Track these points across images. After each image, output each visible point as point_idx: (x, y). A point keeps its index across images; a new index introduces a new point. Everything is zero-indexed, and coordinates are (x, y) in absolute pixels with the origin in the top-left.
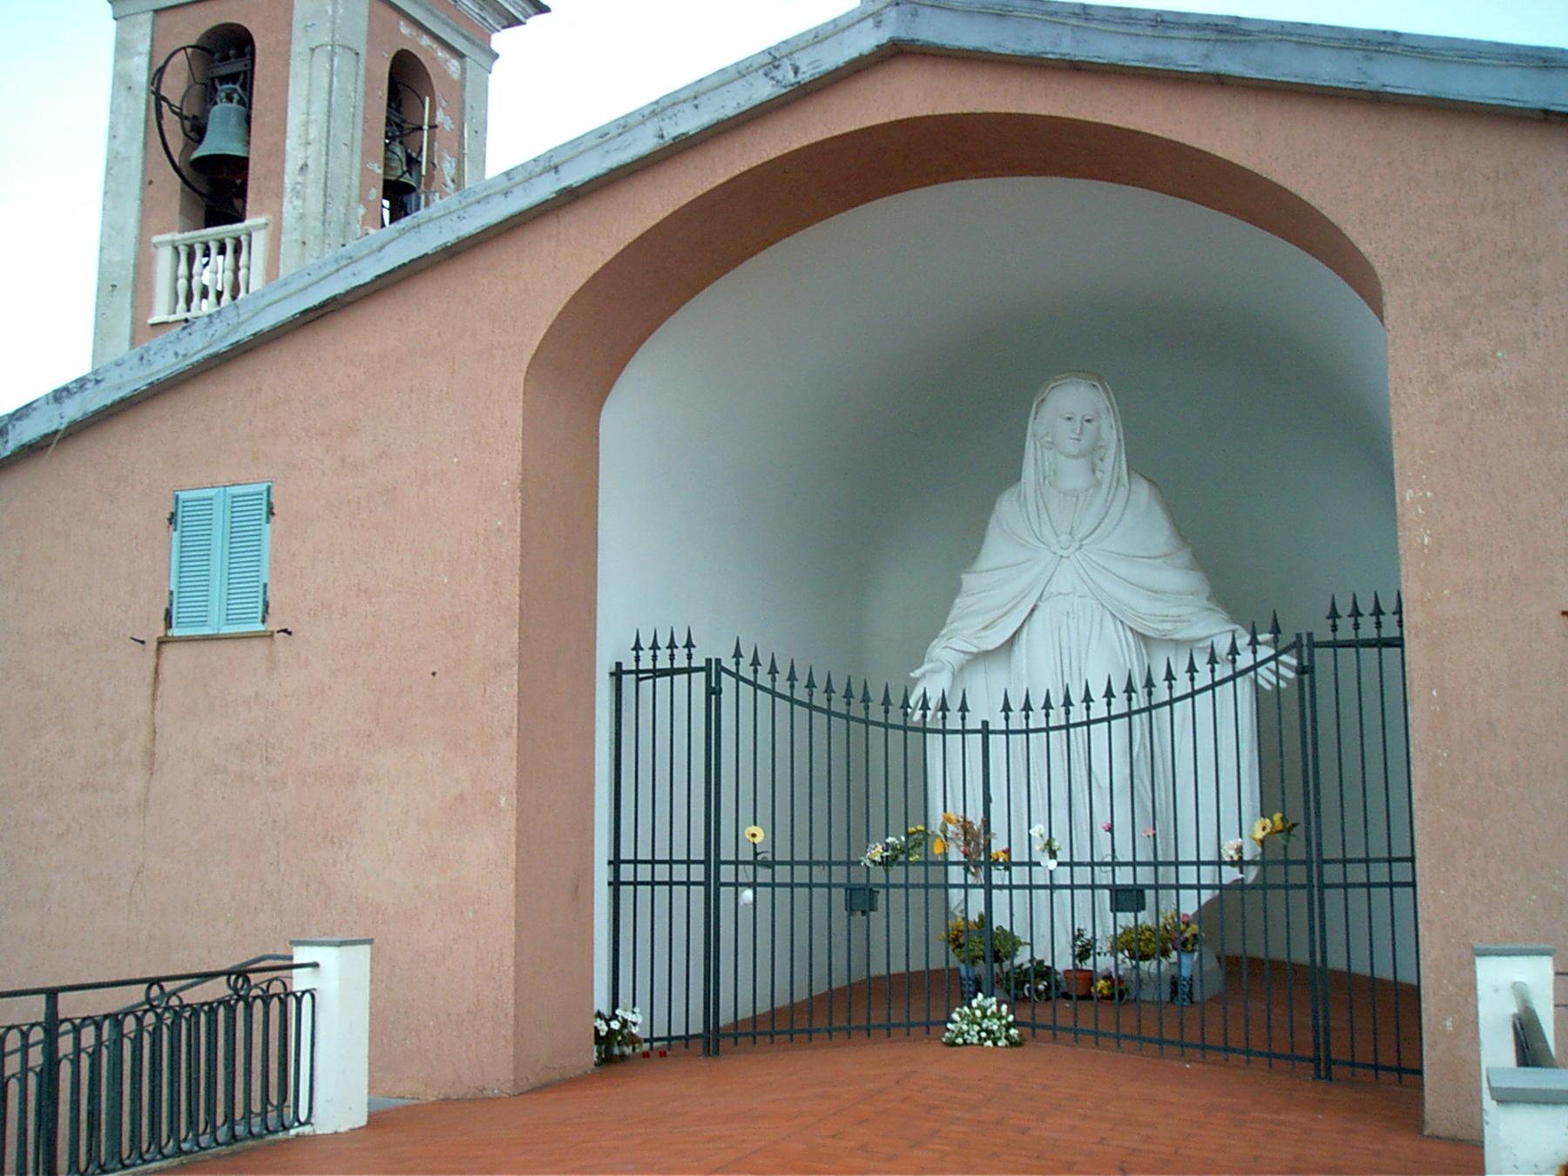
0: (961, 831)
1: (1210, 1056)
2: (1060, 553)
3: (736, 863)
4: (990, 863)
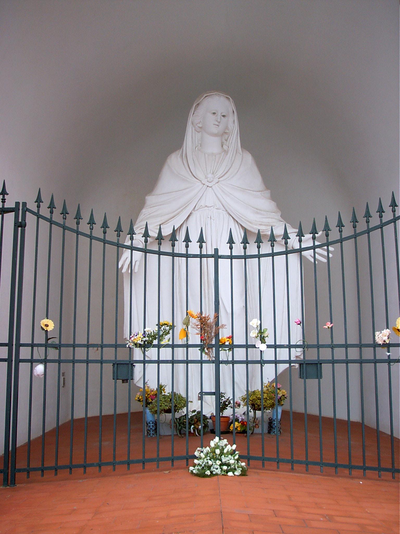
0: (199, 323)
1: (355, 473)
2: (207, 184)
3: (32, 345)
4: (220, 345)
